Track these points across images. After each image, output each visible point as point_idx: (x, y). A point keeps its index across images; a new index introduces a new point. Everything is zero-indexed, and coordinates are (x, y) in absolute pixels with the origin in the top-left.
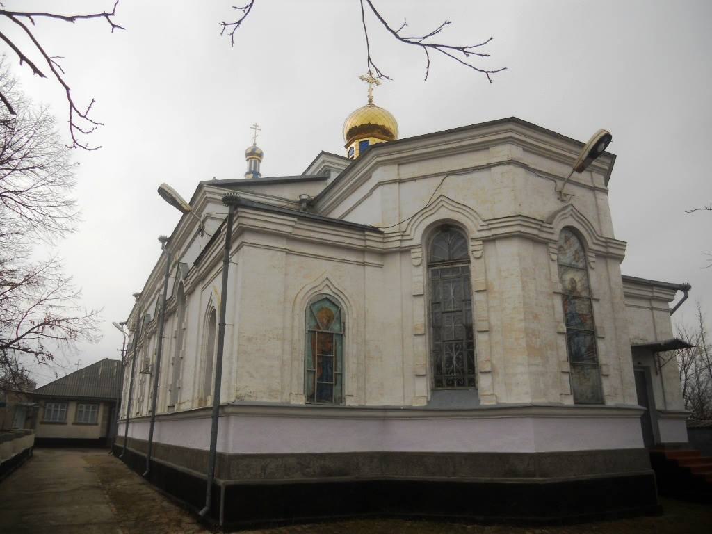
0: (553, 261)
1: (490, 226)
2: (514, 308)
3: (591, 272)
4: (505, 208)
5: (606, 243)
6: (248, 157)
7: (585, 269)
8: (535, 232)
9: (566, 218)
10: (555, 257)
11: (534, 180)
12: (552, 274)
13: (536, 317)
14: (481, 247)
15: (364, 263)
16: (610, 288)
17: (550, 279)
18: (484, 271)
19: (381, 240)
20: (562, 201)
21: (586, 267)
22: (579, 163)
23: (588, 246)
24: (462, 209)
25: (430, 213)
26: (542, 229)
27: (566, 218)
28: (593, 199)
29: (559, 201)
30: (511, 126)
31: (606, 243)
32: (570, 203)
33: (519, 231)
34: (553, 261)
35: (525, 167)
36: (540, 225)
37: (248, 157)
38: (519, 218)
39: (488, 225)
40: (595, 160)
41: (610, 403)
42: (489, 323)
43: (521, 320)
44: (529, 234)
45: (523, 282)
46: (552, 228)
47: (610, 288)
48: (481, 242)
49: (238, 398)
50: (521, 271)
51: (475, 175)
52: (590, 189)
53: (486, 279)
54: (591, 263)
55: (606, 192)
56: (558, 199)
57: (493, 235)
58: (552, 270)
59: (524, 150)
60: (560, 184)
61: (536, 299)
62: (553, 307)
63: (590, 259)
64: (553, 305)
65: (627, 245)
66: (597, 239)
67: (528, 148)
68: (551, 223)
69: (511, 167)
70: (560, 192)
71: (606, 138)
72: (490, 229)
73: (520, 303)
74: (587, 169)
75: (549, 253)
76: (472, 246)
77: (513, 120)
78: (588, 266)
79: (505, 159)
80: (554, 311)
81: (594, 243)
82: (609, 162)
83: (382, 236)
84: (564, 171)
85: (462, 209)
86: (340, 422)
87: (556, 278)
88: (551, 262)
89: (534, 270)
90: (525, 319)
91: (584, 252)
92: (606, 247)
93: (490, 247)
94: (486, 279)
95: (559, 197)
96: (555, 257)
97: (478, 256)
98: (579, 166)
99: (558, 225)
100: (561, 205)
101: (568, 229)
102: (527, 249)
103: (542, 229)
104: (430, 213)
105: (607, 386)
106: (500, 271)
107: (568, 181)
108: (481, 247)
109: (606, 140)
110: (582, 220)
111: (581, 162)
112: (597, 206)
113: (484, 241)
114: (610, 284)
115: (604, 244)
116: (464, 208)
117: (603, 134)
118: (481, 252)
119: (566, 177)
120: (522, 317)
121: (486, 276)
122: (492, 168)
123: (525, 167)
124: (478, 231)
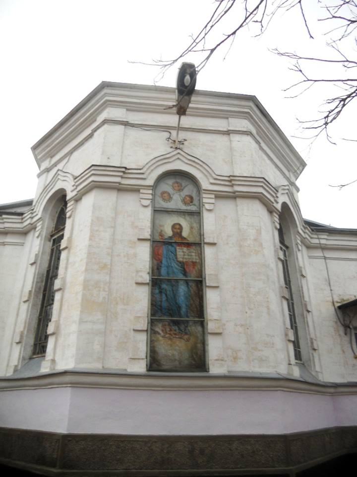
6: (46, 164)
7: (196, 215)
14: (213, 201)
15: (3, 243)
19: (20, 221)
24: (201, 166)
25: (51, 187)
31: (230, 181)
37: (46, 164)
40: (193, 95)
41: (215, 369)
48: (213, 196)
49: (229, 372)
50: (92, 220)
59: (127, 110)
69: (106, 126)
76: (207, 199)
81: (212, 184)
83: (20, 217)
85: (201, 166)
86: (132, 391)
92: (232, 186)
104: (51, 187)
105: (214, 348)
107: (179, 128)
116: (204, 165)
119: (177, 126)
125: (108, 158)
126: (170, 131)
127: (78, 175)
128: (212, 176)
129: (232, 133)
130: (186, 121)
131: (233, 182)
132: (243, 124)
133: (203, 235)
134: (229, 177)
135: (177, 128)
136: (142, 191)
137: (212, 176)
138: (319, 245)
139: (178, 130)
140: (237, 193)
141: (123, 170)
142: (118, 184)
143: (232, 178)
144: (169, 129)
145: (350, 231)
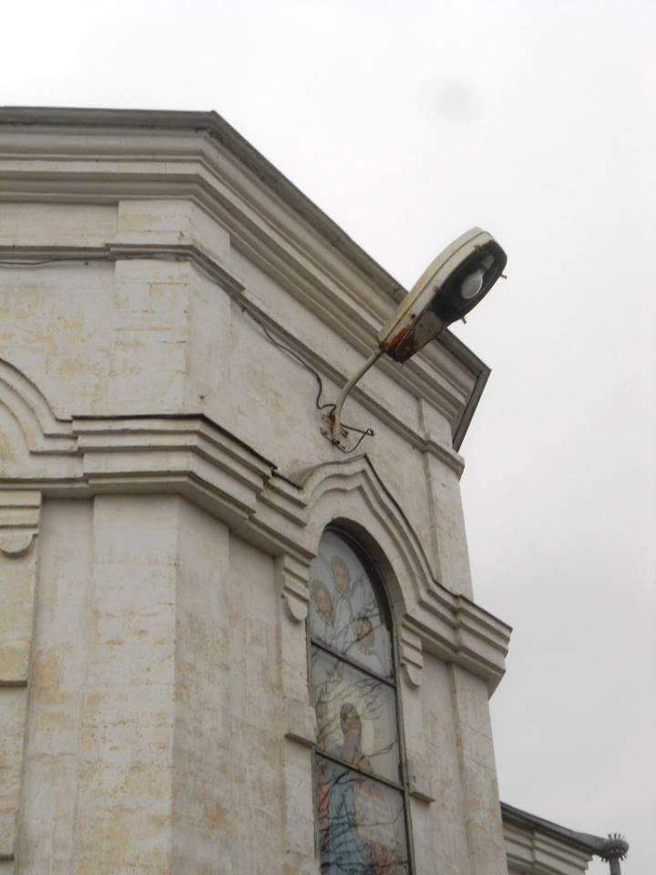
0: (294, 621)
1: (84, 442)
2: (136, 768)
3: (404, 693)
4: (152, 385)
5: (455, 612)
7: (390, 682)
8: (247, 498)
9: (343, 491)
10: (300, 610)
11: (250, 339)
12: (287, 669)
13: (217, 816)
14: (32, 517)
16: (461, 768)
17: (279, 686)
18: (28, 606)
20: (335, 443)
21: (393, 675)
22: (403, 325)
23: (403, 606)
26: (267, 494)
27: (343, 491)
28: (422, 479)
29: (323, 441)
30: (199, 142)
31: (455, 612)
32: (360, 451)
33: (191, 475)
34: (294, 621)
35: (234, 290)
36: (265, 478)
38: (197, 426)
39: (74, 436)
42: (20, 826)
43: (159, 821)
44: (219, 179)
45: (179, 666)
46: (301, 505)
47: (461, 768)
48: (35, 499)
50: (178, 622)
51: (56, 277)
52: (414, 446)
53: (33, 642)
54: (410, 669)
55: (457, 467)
56: (324, 434)
57: (87, 477)
58: (287, 655)
60: (331, 393)
61: (224, 746)
62: (281, 792)
63: (408, 653)
64: (283, 786)
65: (513, 636)
66: (431, 593)
67: (248, 243)
68: (299, 488)
69: (186, 269)
70: (332, 417)
71: (482, 264)
72: (79, 454)
73: (162, 747)
74: (419, 353)
75: (283, 592)
77: (210, 126)
78: (400, 676)
79: (173, 240)
80: (284, 808)
81: (422, 604)
82: (470, 384)
84: (347, 361)
87: (297, 683)
88: (286, 628)
89: (225, 632)
90: (175, 818)
91: (390, 627)
92: (454, 627)
93: (66, 525)
94: (33, 642)
95: (326, 427)
96: (300, 610)
97: (15, 548)
98: (400, 336)
99: (321, 514)
100: (330, 454)
101: (343, 531)
102: (210, 552)
103: (267, 494)
106: (97, 614)
108: (32, 517)
109: (489, 262)
110: (390, 515)
111: (407, 322)
112: (431, 502)
113: (48, 499)
114: (460, 756)
115: (449, 616)
117: (482, 241)
118: (30, 533)
119: (351, 376)
120: (164, 806)
121: (35, 630)
122: (118, 263)
123: (234, 290)
124: (33, 454)
125: (202, 397)
126: (321, 376)
127: (476, 602)
128: (426, 584)
129: (433, 453)
130: (378, 385)
131: (463, 619)
132: (173, 220)
133: (406, 765)
134: (456, 597)
135: (347, 386)
136: (288, 562)
137: (426, 584)
138: (529, 866)
139: (348, 393)
140: (463, 654)
141: (267, 471)
142: (185, 479)
143: (463, 604)
144: (325, 373)
145: (526, 820)
